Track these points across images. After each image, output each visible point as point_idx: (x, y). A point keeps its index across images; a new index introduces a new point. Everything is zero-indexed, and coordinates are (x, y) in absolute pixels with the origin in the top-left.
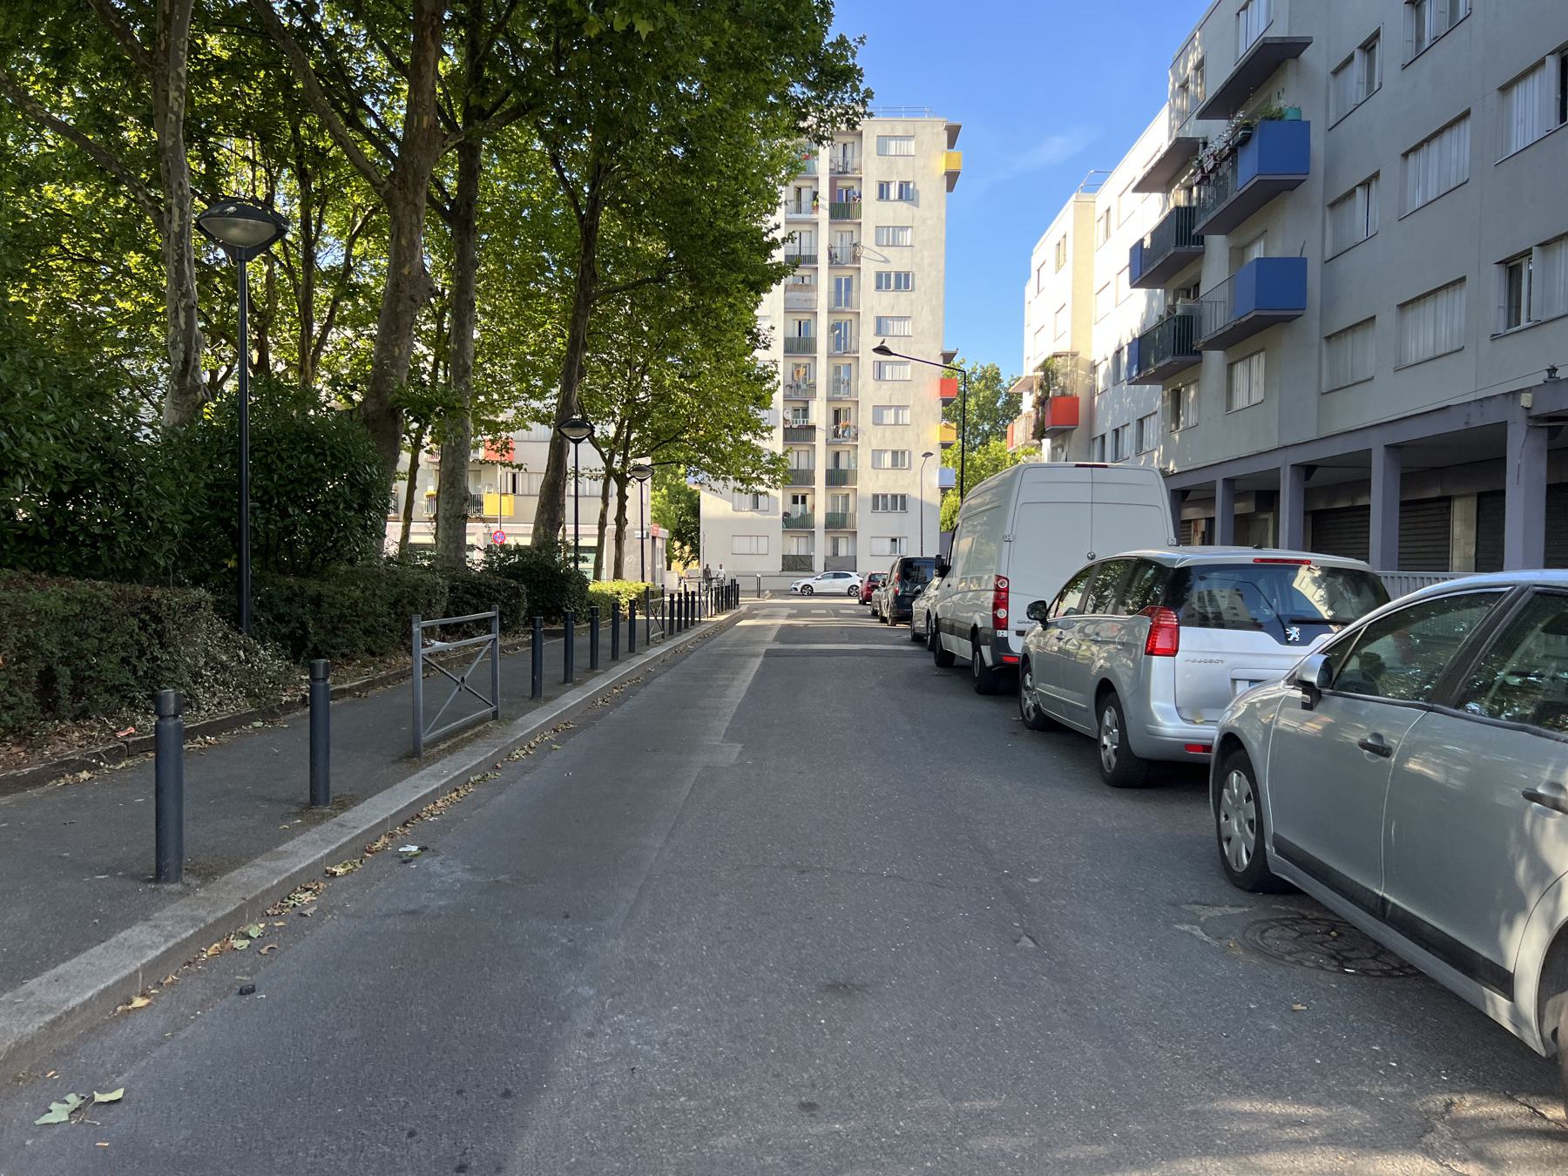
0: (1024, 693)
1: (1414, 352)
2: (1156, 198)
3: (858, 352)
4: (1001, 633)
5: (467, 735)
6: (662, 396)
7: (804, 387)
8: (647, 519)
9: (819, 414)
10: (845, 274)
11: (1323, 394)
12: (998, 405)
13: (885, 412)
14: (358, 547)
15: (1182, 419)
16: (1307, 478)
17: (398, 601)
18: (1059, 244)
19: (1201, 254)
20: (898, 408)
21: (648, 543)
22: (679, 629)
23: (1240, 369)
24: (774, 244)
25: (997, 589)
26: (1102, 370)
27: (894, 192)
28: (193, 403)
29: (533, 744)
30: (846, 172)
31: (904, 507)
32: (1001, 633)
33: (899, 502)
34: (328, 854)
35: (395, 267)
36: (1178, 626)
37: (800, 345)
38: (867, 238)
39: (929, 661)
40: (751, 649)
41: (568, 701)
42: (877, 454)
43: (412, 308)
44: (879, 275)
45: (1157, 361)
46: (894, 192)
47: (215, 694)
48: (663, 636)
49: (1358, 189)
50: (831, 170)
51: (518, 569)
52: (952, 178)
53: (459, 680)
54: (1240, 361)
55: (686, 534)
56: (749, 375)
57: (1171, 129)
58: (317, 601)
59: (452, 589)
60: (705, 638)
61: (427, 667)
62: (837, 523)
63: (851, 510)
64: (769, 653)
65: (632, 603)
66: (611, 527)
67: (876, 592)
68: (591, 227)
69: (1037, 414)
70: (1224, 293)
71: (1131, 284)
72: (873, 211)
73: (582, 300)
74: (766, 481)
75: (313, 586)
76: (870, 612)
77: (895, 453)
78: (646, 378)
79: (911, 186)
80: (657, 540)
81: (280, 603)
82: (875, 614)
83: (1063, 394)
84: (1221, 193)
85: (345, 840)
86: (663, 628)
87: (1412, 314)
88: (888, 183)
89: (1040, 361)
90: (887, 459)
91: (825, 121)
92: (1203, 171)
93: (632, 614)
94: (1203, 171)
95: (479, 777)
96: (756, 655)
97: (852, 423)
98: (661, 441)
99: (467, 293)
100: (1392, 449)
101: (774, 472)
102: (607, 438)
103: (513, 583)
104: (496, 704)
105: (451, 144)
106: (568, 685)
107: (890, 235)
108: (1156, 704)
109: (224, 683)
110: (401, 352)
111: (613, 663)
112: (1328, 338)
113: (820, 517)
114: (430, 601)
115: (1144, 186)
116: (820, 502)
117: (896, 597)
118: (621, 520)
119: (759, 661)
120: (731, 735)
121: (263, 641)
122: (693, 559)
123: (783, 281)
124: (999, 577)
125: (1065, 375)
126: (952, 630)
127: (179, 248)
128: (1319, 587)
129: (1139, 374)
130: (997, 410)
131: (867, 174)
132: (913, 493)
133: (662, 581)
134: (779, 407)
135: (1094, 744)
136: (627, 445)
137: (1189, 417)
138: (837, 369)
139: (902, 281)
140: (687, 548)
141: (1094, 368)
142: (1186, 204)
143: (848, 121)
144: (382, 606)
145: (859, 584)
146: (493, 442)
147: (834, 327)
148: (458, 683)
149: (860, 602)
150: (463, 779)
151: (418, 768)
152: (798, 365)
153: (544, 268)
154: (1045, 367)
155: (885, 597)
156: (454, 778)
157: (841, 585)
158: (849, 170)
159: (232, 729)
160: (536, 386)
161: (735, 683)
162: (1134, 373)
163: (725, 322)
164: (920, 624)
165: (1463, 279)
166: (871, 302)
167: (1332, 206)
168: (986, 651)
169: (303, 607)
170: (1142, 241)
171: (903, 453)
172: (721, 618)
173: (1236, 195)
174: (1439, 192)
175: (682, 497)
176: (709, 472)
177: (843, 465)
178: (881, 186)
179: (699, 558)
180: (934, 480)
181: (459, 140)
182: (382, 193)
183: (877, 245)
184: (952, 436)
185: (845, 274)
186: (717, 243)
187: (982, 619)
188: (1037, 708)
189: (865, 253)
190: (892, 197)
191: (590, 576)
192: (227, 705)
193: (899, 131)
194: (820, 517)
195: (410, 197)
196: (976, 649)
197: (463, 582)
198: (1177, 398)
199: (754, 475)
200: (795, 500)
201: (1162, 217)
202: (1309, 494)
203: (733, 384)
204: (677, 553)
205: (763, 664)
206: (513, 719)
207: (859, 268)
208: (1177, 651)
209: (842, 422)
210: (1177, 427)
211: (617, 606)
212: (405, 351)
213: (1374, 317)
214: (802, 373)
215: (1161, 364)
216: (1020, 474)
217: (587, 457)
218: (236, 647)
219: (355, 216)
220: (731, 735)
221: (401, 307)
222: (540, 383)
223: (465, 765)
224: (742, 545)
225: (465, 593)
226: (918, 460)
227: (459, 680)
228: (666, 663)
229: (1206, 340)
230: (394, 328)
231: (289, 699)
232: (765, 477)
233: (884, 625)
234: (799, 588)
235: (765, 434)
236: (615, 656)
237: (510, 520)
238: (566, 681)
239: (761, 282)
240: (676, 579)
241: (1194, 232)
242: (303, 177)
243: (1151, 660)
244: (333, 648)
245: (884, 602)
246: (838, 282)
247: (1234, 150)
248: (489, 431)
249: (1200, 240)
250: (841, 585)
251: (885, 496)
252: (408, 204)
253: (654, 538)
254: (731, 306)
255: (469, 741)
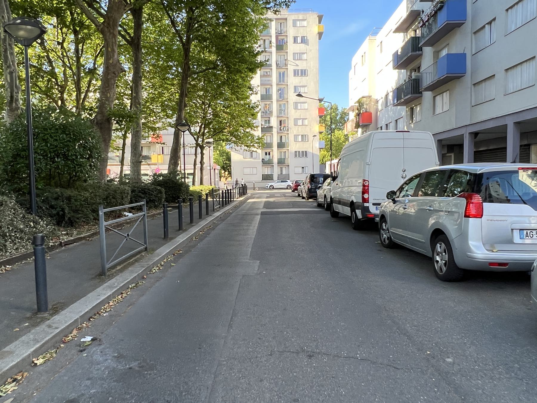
0: (382, 232)
1: (511, 88)
2: (402, 34)
3: (288, 99)
4: (366, 205)
5: (131, 260)
6: (216, 115)
7: (268, 112)
8: (212, 163)
9: (274, 122)
10: (282, 71)
11: (473, 106)
12: (337, 118)
13: (298, 121)
14: (87, 175)
15: (414, 119)
16: (475, 137)
17: (107, 197)
18: (362, 56)
19: (421, 55)
20: (303, 119)
21: (212, 171)
22: (226, 204)
23: (438, 98)
24: (258, 53)
25: (364, 186)
26: (380, 103)
27: (299, 40)
28: (17, 115)
29: (163, 263)
30: (281, 33)
31: (306, 156)
32: (366, 205)
33: (305, 154)
34: (34, 351)
35: (106, 60)
36: (482, 203)
37: (266, 97)
38: (290, 57)
39: (328, 215)
40: (254, 212)
41: (179, 239)
42: (296, 136)
43: (114, 77)
44: (295, 71)
45: (405, 96)
46: (299, 40)
47: (15, 244)
48: (220, 207)
49: (486, 26)
50: (276, 33)
51: (162, 182)
52: (320, 34)
53: (126, 235)
54: (438, 95)
55: (226, 168)
56: (249, 106)
57: (407, 8)
58: (69, 198)
59: (133, 191)
60: (236, 207)
61: (107, 230)
62: (281, 162)
63: (287, 157)
64: (262, 213)
65: (207, 195)
66: (198, 165)
67: (299, 187)
68: (187, 48)
69: (356, 119)
70: (431, 70)
71: (393, 67)
72: (292, 48)
73: (185, 77)
74: (256, 146)
75: (68, 192)
76: (297, 195)
77: (302, 136)
78: (210, 109)
79: (306, 38)
80: (216, 170)
81: (52, 200)
82: (299, 195)
83: (366, 112)
84: (430, 30)
85: (47, 339)
86: (219, 204)
87: (510, 72)
88: (297, 37)
89: (357, 100)
90: (300, 138)
91: (278, 5)
92: (423, 22)
93: (207, 198)
94: (423, 22)
95: (133, 285)
96: (257, 214)
97: (286, 125)
98: (217, 132)
99: (139, 74)
100: (517, 124)
101: (259, 143)
102: (196, 132)
103: (159, 188)
104: (146, 243)
105: (128, 9)
106: (181, 231)
107: (298, 56)
108: (472, 243)
109: (21, 238)
110: (110, 95)
111: (201, 220)
112: (474, 85)
113: (275, 161)
114: (122, 197)
115: (398, 30)
116: (275, 155)
117: (309, 189)
118: (202, 163)
119: (259, 217)
120: (254, 256)
121: (41, 217)
122: (229, 177)
123: (258, 71)
124: (364, 180)
125: (367, 104)
126: (339, 202)
127: (4, 45)
128: (533, 180)
129: (397, 101)
130: (337, 120)
131: (289, 34)
132: (310, 150)
133: (218, 185)
134: (259, 120)
135: (431, 260)
136: (203, 134)
137: (417, 117)
138: (280, 105)
139: (304, 73)
140: (227, 173)
141: (377, 101)
142: (414, 36)
143: (286, 4)
144: (100, 200)
145: (291, 185)
146: (154, 135)
147: (278, 90)
148: (126, 237)
149: (292, 191)
150: (125, 287)
151: (103, 282)
152: (266, 104)
153: (171, 67)
154: (359, 102)
155: (304, 189)
156: (120, 287)
157: (284, 185)
158: (283, 32)
159: (22, 260)
160: (169, 114)
161: (251, 228)
162: (395, 102)
163: (240, 84)
164: (321, 200)
165: (534, 57)
166: (292, 81)
167: (475, 33)
168: (359, 212)
169: (63, 201)
170: (398, 51)
171: (305, 136)
172: (241, 199)
173: (437, 30)
174: (516, 24)
175: (224, 154)
176: (235, 143)
177: (283, 141)
178: (295, 38)
179: (231, 176)
180: (317, 145)
181: (131, 7)
182: (100, 30)
183: (294, 60)
184: (323, 129)
185: (282, 71)
186: (236, 53)
187: (357, 198)
188: (389, 238)
189: (289, 63)
190: (299, 42)
191: (191, 184)
192: (21, 249)
193: (301, 18)
194: (275, 161)
195: (112, 31)
196: (353, 210)
197: (138, 188)
198: (412, 109)
199: (252, 144)
200: (266, 154)
201: (404, 43)
202: (476, 144)
203: (243, 110)
204: (223, 175)
205: (261, 219)
206: (154, 250)
207: (287, 69)
208: (482, 216)
209: (283, 125)
210: (412, 122)
211: (200, 197)
212: (112, 95)
213: (494, 75)
214: (267, 108)
215: (406, 97)
216: (372, 135)
217: (187, 139)
218: (29, 221)
219: (97, 48)
220: (254, 256)
221: (109, 77)
222: (171, 112)
223: (128, 279)
224: (247, 171)
225: (139, 192)
226: (311, 138)
227: (126, 235)
228: (221, 219)
229: (425, 87)
230: (107, 85)
231: (53, 244)
232: (256, 145)
233: (304, 200)
234: (269, 186)
235: (255, 129)
236: (200, 217)
237: (161, 164)
238: (179, 230)
239: (253, 68)
240: (223, 185)
241: (420, 46)
242: (76, 33)
243: (468, 221)
244: (78, 219)
245: (304, 191)
246: (280, 73)
247: (434, 15)
248: (152, 131)
249: (421, 49)
250: (284, 185)
251: (299, 152)
252: (110, 34)
253: (215, 169)
254: (242, 78)
255: (132, 264)
